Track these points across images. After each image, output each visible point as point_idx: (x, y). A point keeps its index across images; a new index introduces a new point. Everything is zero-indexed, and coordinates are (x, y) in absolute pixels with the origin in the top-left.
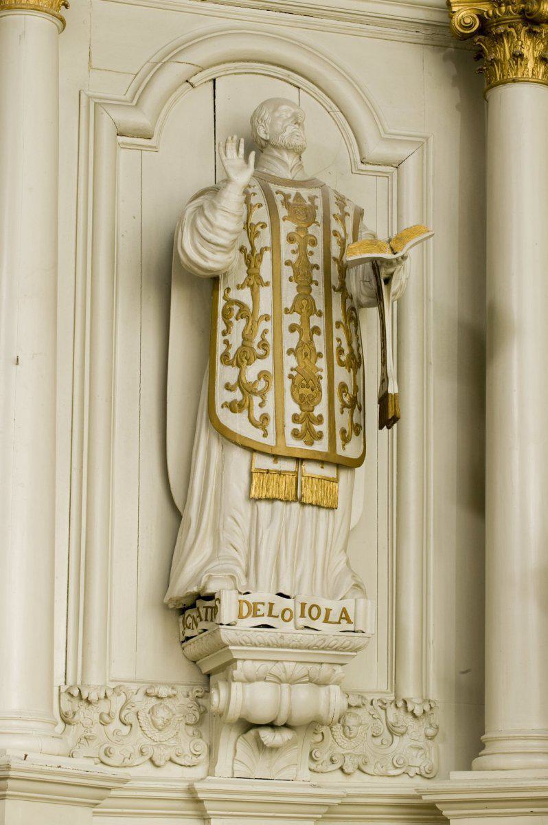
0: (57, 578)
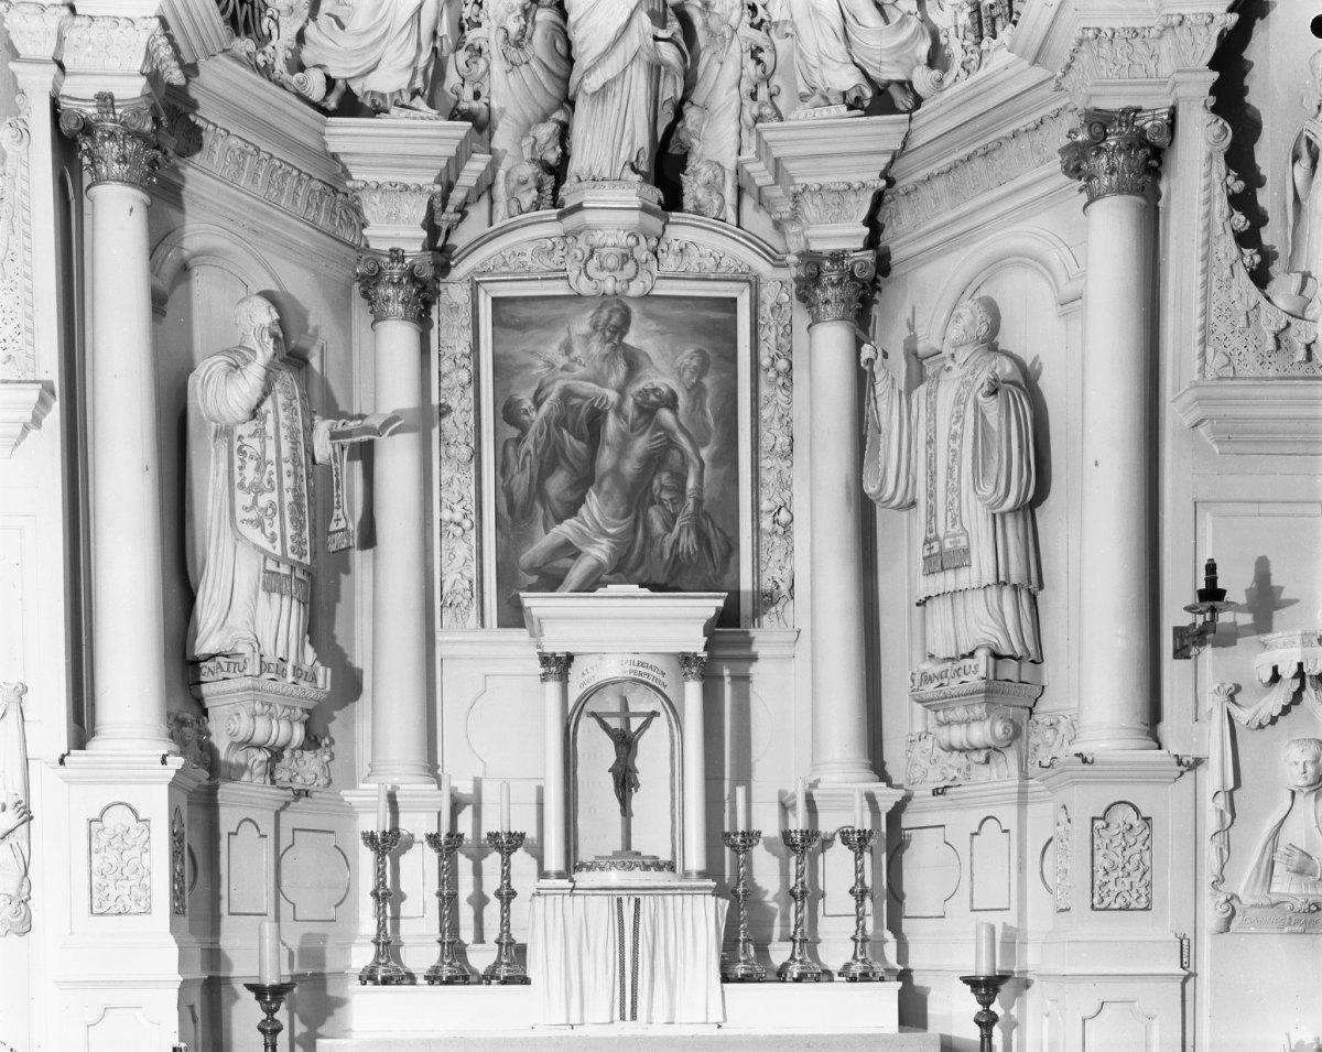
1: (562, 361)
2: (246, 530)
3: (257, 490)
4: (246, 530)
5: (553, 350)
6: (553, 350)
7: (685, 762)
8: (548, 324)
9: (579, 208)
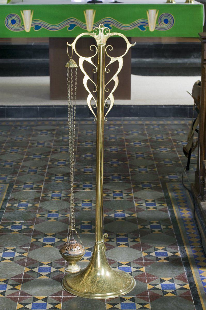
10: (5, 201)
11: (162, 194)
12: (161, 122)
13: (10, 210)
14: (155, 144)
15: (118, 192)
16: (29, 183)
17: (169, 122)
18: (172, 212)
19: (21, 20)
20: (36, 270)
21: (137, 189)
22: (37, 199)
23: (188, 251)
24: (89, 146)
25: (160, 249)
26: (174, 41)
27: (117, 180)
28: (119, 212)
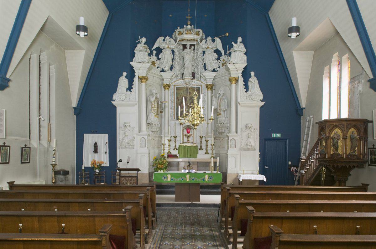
0: (106, 143)
1: (183, 93)
2: (153, 112)
3: (154, 108)
4: (153, 112)
5: (182, 92)
6: (182, 92)
7: (50, 99)
8: (182, 89)
9: (184, 79)
10: (164, 230)
11: (210, 229)
12: (210, 209)
13: (165, 232)
14: (208, 215)
15: (197, 228)
16: (171, 225)
17: (212, 209)
18: (213, 233)
19: (167, 177)
20: (175, 247)
21: (203, 227)
22: (173, 229)
23: (218, 243)
24: (188, 215)
25: (210, 243)
26: (213, 184)
27: (196, 225)
28: (198, 233)
